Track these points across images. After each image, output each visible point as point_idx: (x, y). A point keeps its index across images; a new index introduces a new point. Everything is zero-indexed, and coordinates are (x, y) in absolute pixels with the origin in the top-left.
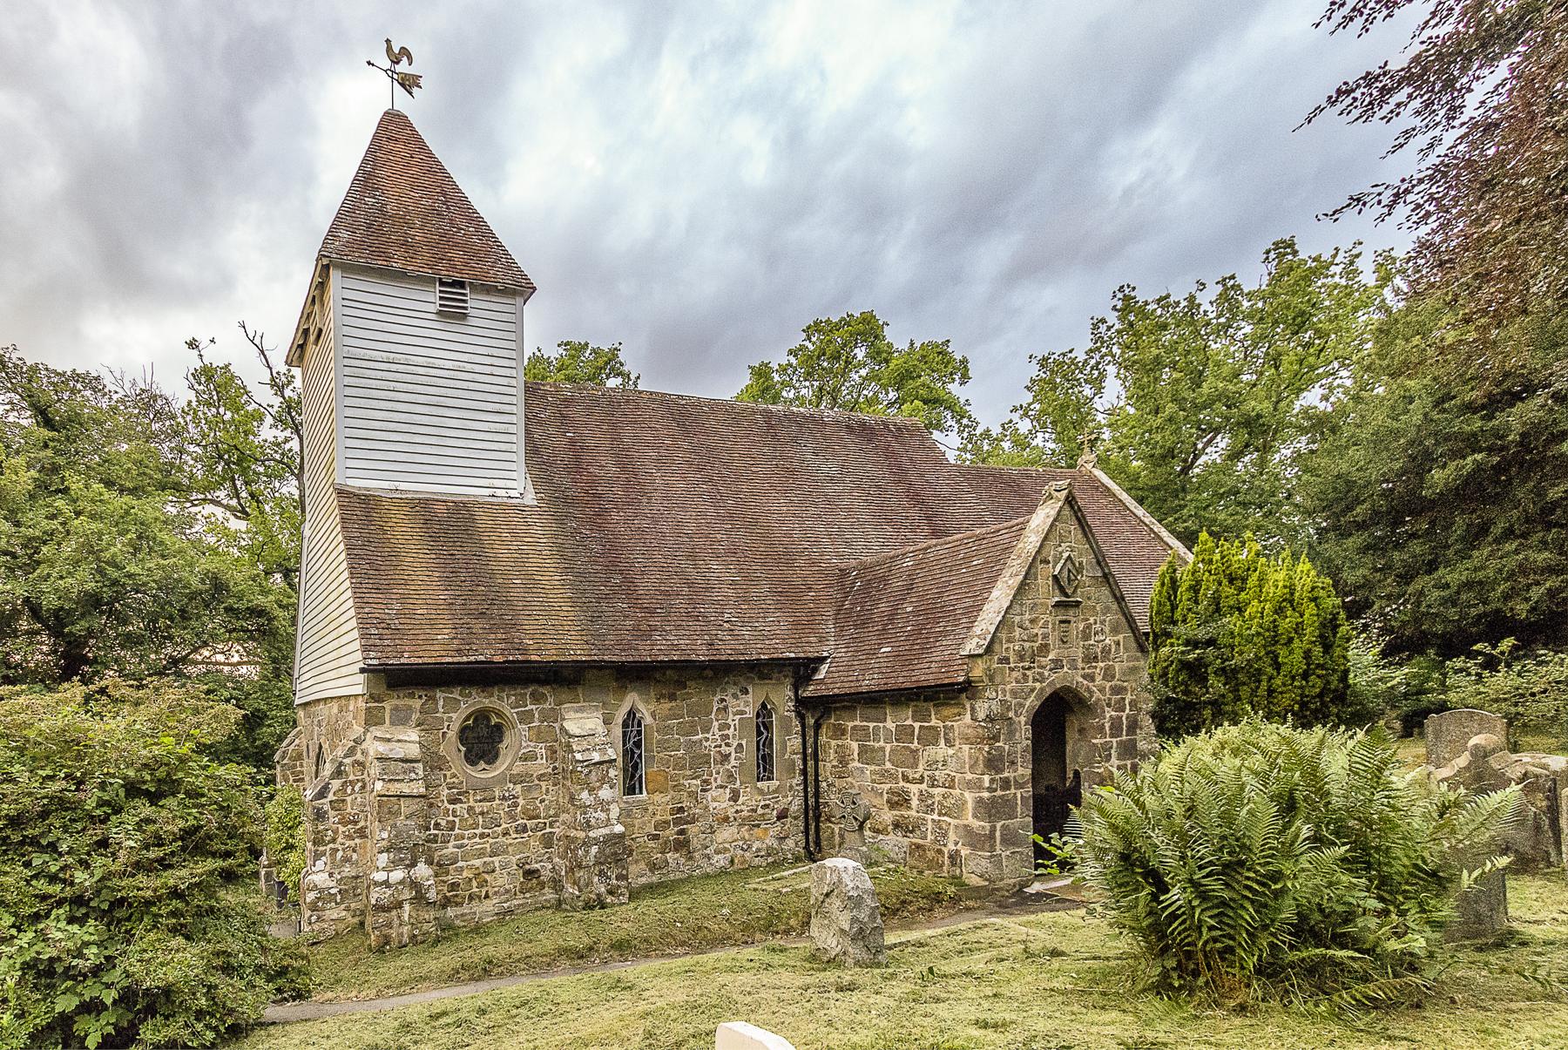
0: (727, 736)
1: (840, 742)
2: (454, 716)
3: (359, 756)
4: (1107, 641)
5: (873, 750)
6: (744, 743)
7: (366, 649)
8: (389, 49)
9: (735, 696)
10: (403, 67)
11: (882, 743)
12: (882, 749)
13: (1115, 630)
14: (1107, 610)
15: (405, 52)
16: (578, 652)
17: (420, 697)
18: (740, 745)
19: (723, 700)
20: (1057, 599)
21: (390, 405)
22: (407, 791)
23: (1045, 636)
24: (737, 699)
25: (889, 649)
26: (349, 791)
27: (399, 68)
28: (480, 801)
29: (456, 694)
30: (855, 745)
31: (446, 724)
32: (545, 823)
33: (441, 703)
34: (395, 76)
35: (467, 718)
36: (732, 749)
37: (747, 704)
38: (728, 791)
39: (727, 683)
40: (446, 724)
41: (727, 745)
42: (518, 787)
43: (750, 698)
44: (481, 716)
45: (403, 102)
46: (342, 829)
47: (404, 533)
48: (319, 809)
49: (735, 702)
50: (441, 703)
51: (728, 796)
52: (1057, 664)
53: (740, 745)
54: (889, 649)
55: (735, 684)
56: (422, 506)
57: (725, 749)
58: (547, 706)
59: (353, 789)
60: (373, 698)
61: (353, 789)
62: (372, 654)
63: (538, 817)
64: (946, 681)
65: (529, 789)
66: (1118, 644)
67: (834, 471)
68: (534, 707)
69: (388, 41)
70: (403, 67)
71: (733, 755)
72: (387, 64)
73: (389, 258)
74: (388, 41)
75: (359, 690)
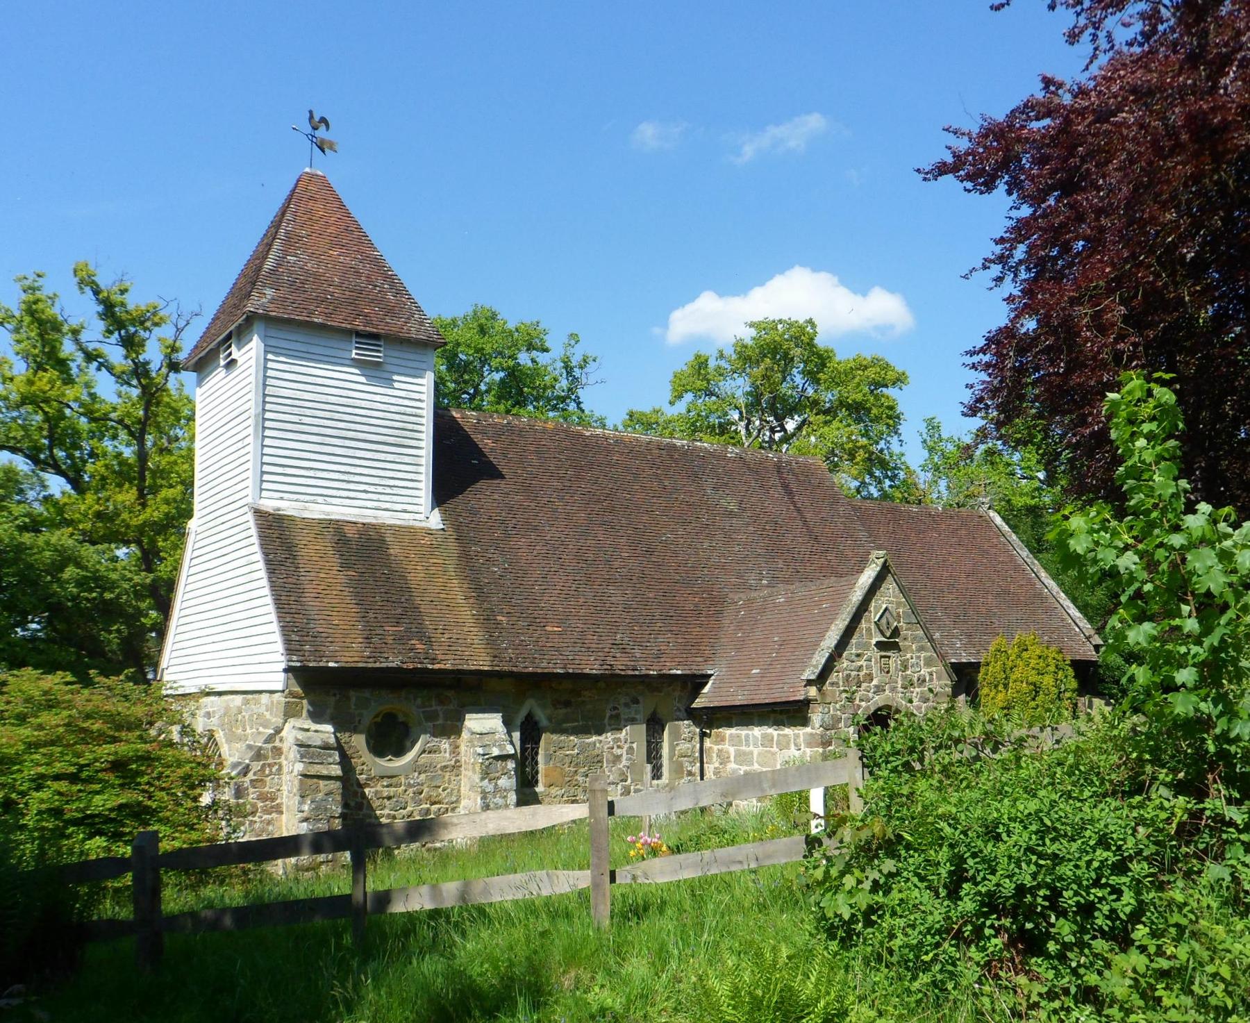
0: (619, 740)
1: (720, 747)
2: (365, 712)
3: (277, 744)
4: (922, 672)
5: (744, 753)
6: (635, 745)
7: (289, 651)
8: (311, 117)
9: (626, 705)
10: (321, 133)
11: (751, 748)
12: (751, 753)
13: (929, 663)
14: (921, 649)
15: (323, 120)
16: (481, 661)
17: (335, 695)
18: (631, 748)
19: (615, 708)
20: (877, 639)
21: (304, 437)
22: (325, 772)
23: (868, 667)
24: (629, 708)
25: (758, 671)
26: (267, 772)
27: (317, 133)
28: (387, 786)
29: (367, 694)
30: (732, 750)
31: (357, 719)
32: (447, 809)
33: (353, 699)
34: (314, 140)
35: (377, 716)
36: (624, 751)
37: (637, 712)
38: (619, 787)
39: (619, 693)
40: (357, 719)
41: (619, 747)
42: (423, 776)
43: (640, 706)
44: (390, 718)
45: (322, 166)
46: (260, 804)
47: (311, 551)
48: (239, 786)
49: (627, 710)
50: (353, 699)
51: (619, 792)
52: (879, 689)
53: (631, 748)
54: (758, 671)
55: (627, 694)
56: (336, 531)
57: (617, 751)
58: (451, 707)
59: (271, 771)
60: (292, 695)
61: (271, 771)
62: (295, 658)
63: (439, 802)
64: (792, 699)
65: (432, 778)
66: (931, 674)
67: (733, 507)
68: (439, 708)
69: (311, 112)
70: (321, 133)
71: (625, 756)
72: (309, 130)
73: (311, 313)
74: (311, 112)
75: (280, 687)
